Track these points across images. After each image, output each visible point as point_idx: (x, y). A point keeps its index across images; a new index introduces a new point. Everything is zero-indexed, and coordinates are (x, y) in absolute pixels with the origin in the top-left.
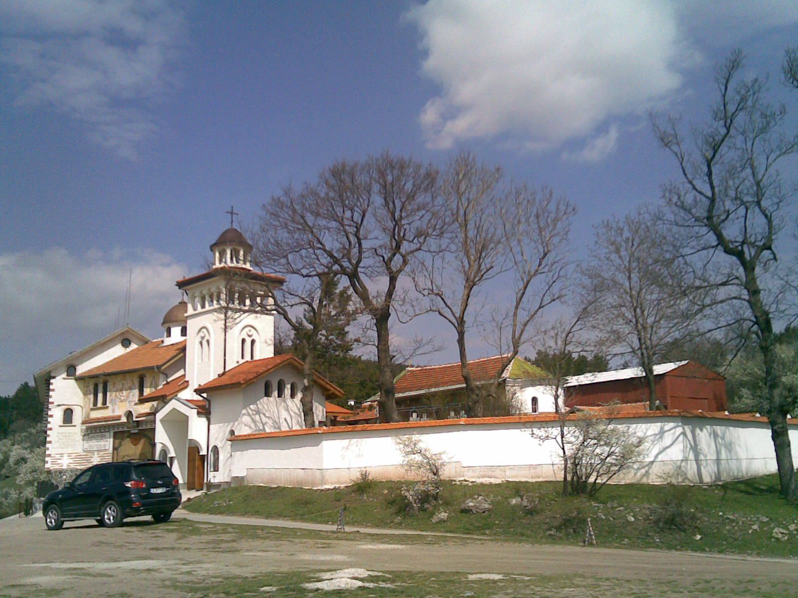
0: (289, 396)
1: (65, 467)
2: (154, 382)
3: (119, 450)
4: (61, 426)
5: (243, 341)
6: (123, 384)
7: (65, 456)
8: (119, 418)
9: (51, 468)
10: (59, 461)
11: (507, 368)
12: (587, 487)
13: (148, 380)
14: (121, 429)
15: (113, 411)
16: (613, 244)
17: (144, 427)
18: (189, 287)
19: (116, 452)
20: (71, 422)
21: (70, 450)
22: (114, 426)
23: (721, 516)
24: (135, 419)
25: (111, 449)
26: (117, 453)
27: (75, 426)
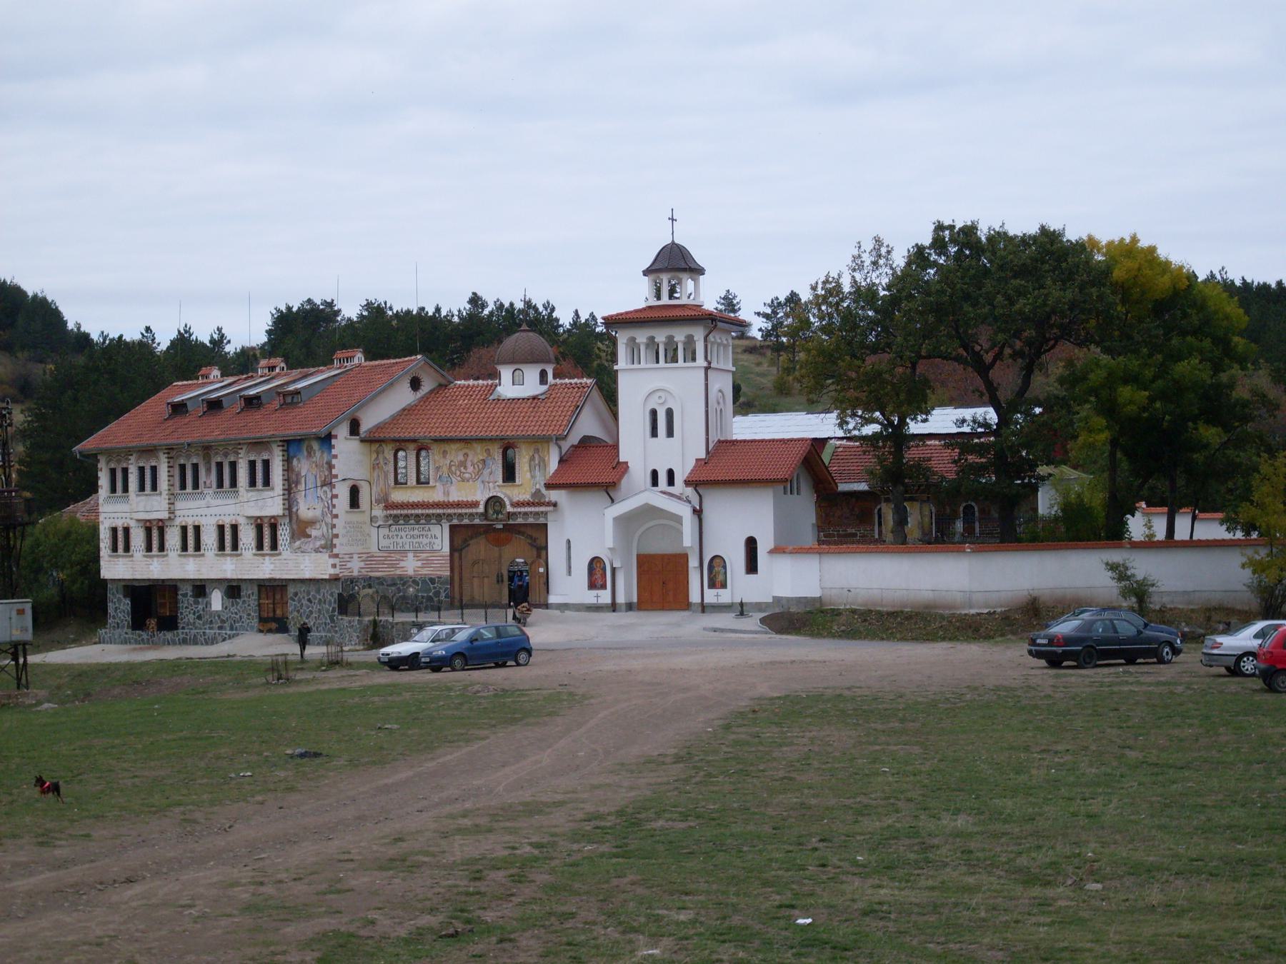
0: (109, 552)
1: (355, 574)
2: (537, 456)
3: (464, 551)
4: (347, 512)
5: (654, 413)
6: (466, 455)
7: (355, 556)
8: (475, 504)
9: (341, 575)
10: (349, 565)
11: (440, 651)
12: (980, 238)
13: (524, 452)
14: (466, 521)
15: (447, 493)
16: (582, 875)
17: (520, 521)
18: (619, 328)
19: (456, 555)
20: (358, 507)
21: (360, 549)
22: (449, 517)
23: (1051, 769)
24: (509, 509)
25: (446, 549)
26: (460, 558)
27: (364, 512)
